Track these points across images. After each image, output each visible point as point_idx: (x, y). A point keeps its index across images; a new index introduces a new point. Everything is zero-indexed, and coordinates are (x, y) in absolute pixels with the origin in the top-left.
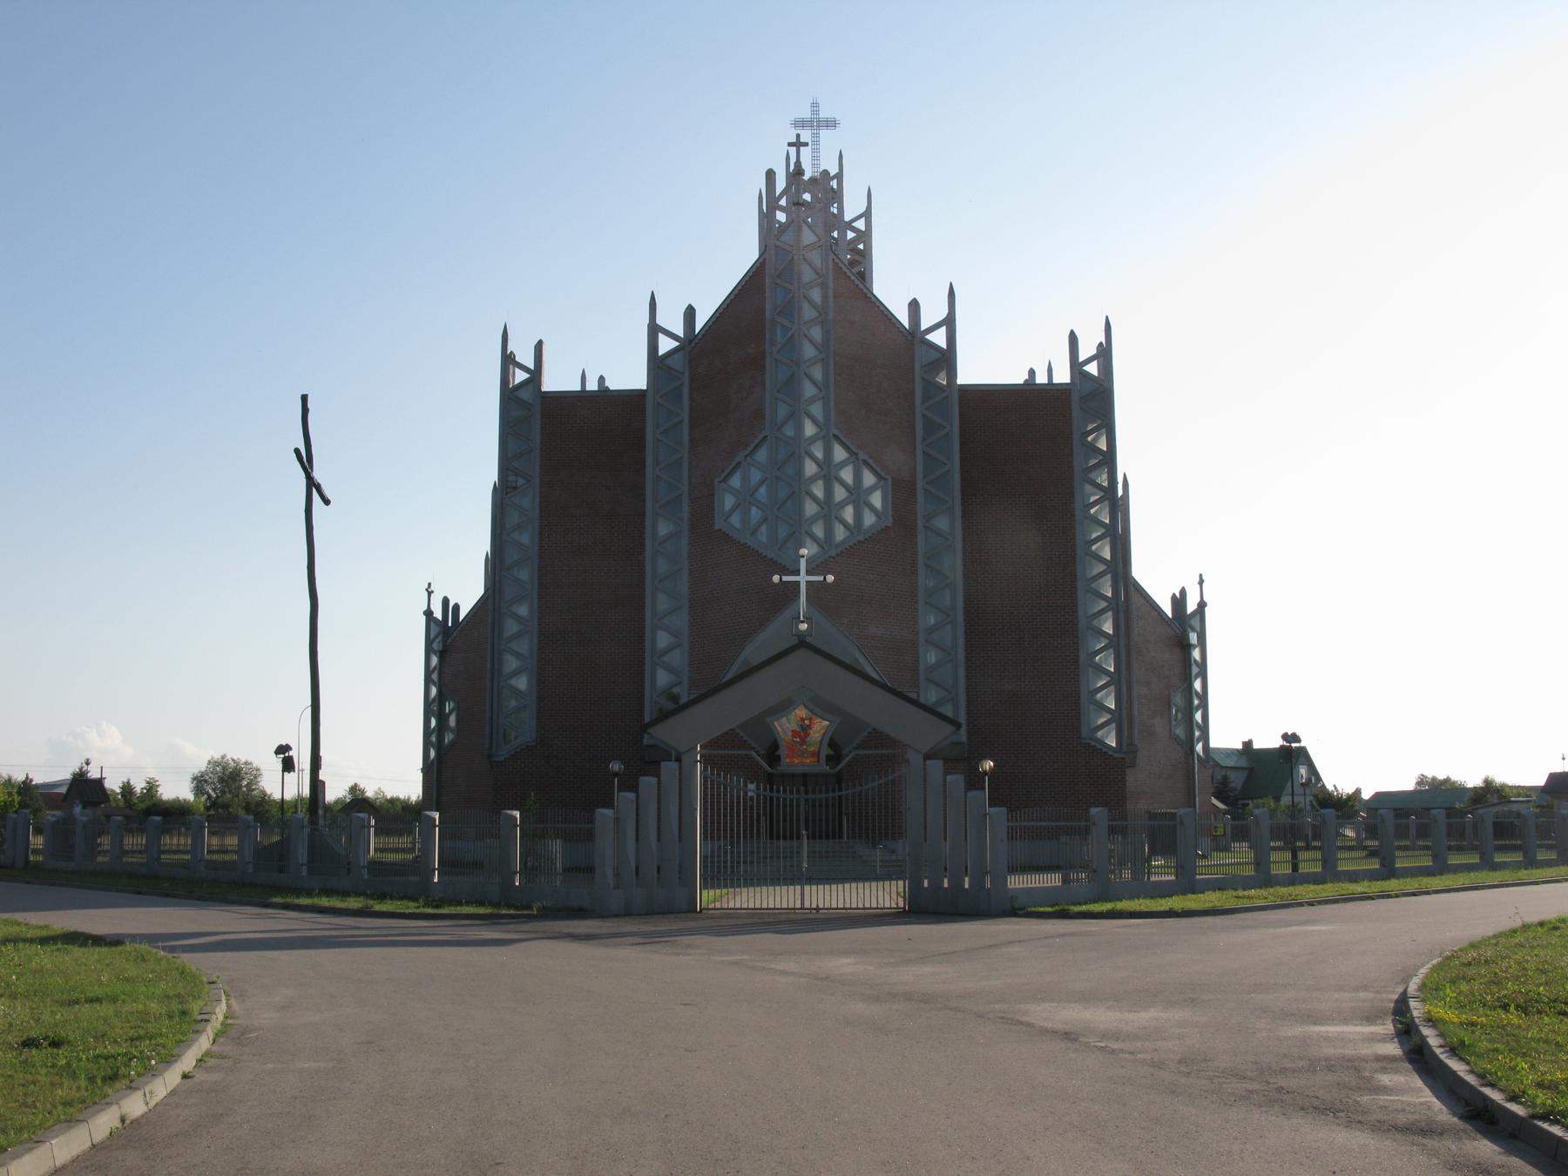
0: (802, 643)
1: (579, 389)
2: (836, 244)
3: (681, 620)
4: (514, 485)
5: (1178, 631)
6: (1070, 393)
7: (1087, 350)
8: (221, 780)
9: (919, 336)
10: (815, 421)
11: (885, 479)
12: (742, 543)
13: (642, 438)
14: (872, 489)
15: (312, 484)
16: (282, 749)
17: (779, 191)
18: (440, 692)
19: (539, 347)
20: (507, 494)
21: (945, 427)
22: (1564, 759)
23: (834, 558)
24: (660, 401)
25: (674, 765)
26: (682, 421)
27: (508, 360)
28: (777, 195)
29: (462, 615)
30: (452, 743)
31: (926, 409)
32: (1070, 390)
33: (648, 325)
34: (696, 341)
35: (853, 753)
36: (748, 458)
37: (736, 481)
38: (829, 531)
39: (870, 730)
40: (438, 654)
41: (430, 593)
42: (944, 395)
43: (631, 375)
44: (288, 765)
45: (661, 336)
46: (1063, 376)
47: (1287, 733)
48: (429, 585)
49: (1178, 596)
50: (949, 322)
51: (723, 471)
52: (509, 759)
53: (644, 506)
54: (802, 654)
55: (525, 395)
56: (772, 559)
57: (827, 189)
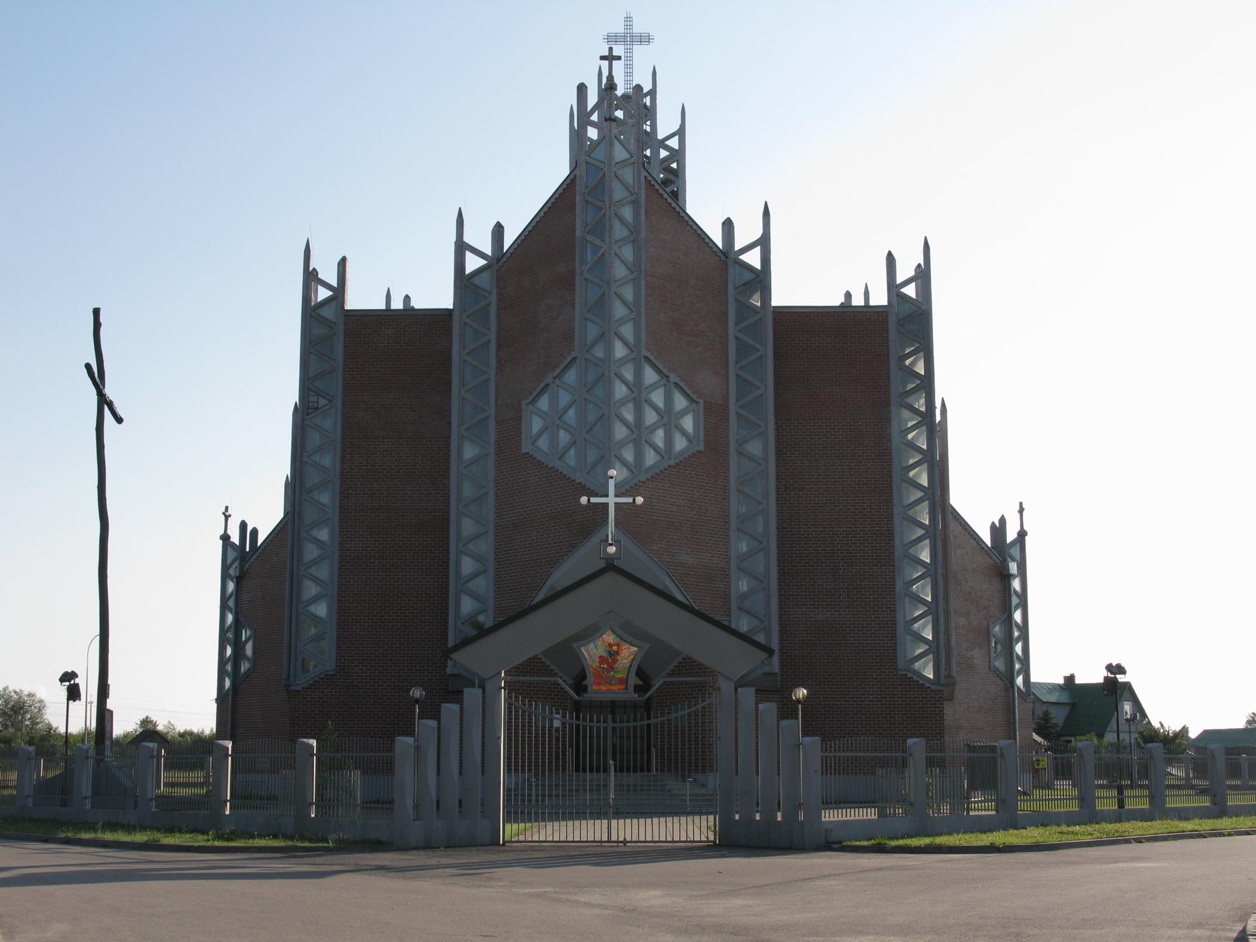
1: (383, 307)
2: (649, 163)
3: (485, 547)
4: (315, 405)
7: (905, 271)
9: (732, 256)
10: (625, 343)
12: (550, 466)
13: (448, 358)
14: (683, 413)
15: (104, 401)
16: (68, 677)
18: (236, 620)
19: (343, 263)
20: (308, 415)
24: (467, 321)
27: (311, 277)
28: (589, 109)
29: (261, 538)
32: (887, 312)
36: (556, 379)
37: (544, 403)
39: (683, 656)
40: (235, 580)
41: (227, 517)
45: (469, 255)
46: (880, 298)
49: (997, 524)
50: (764, 242)
52: (307, 688)
54: (610, 577)
55: (328, 313)
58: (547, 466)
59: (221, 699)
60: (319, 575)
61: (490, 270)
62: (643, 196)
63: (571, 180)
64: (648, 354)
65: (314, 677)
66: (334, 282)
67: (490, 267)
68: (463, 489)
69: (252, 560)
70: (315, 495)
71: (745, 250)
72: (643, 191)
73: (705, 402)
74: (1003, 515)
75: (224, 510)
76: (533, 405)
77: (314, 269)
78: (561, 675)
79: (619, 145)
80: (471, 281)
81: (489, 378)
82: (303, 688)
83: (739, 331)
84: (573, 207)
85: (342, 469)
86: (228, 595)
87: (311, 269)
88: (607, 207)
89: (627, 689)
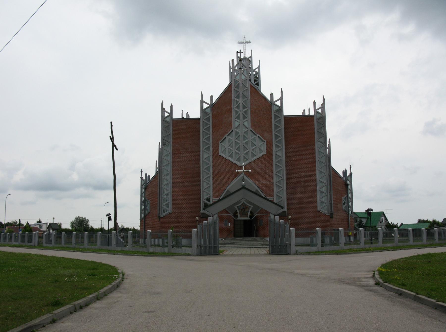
0: (244, 187)
1: (181, 118)
2: (251, 75)
4: (165, 144)
5: (344, 181)
6: (314, 117)
7: (318, 105)
8: (79, 223)
9: (273, 103)
11: (264, 141)
12: (226, 159)
13: (199, 131)
15: (114, 145)
16: (108, 215)
17: (235, 65)
18: (145, 199)
19: (171, 107)
21: (280, 127)
22: (54, 219)
23: (251, 163)
25: (211, 218)
26: (210, 126)
27: (163, 110)
28: (235, 66)
29: (151, 178)
30: (149, 213)
31: (275, 122)
32: (314, 117)
33: (201, 100)
34: (214, 105)
35: (256, 214)
39: (261, 208)
40: (144, 189)
41: (142, 172)
43: (196, 114)
44: (110, 219)
45: (204, 104)
46: (312, 113)
47: (372, 210)
48: (142, 170)
49: (344, 171)
50: (281, 99)
53: (200, 149)
54: (243, 190)
55: (168, 119)
56: (234, 163)
57: (249, 61)
58: (226, 159)
59: (141, 220)
61: (210, 108)
62: (249, 88)
63: (231, 84)
64: (251, 129)
66: (169, 111)
73: (266, 141)
74: (346, 169)
77: (164, 108)
78: (231, 213)
79: (243, 75)
83: (276, 142)
85: (173, 160)
86: (142, 193)
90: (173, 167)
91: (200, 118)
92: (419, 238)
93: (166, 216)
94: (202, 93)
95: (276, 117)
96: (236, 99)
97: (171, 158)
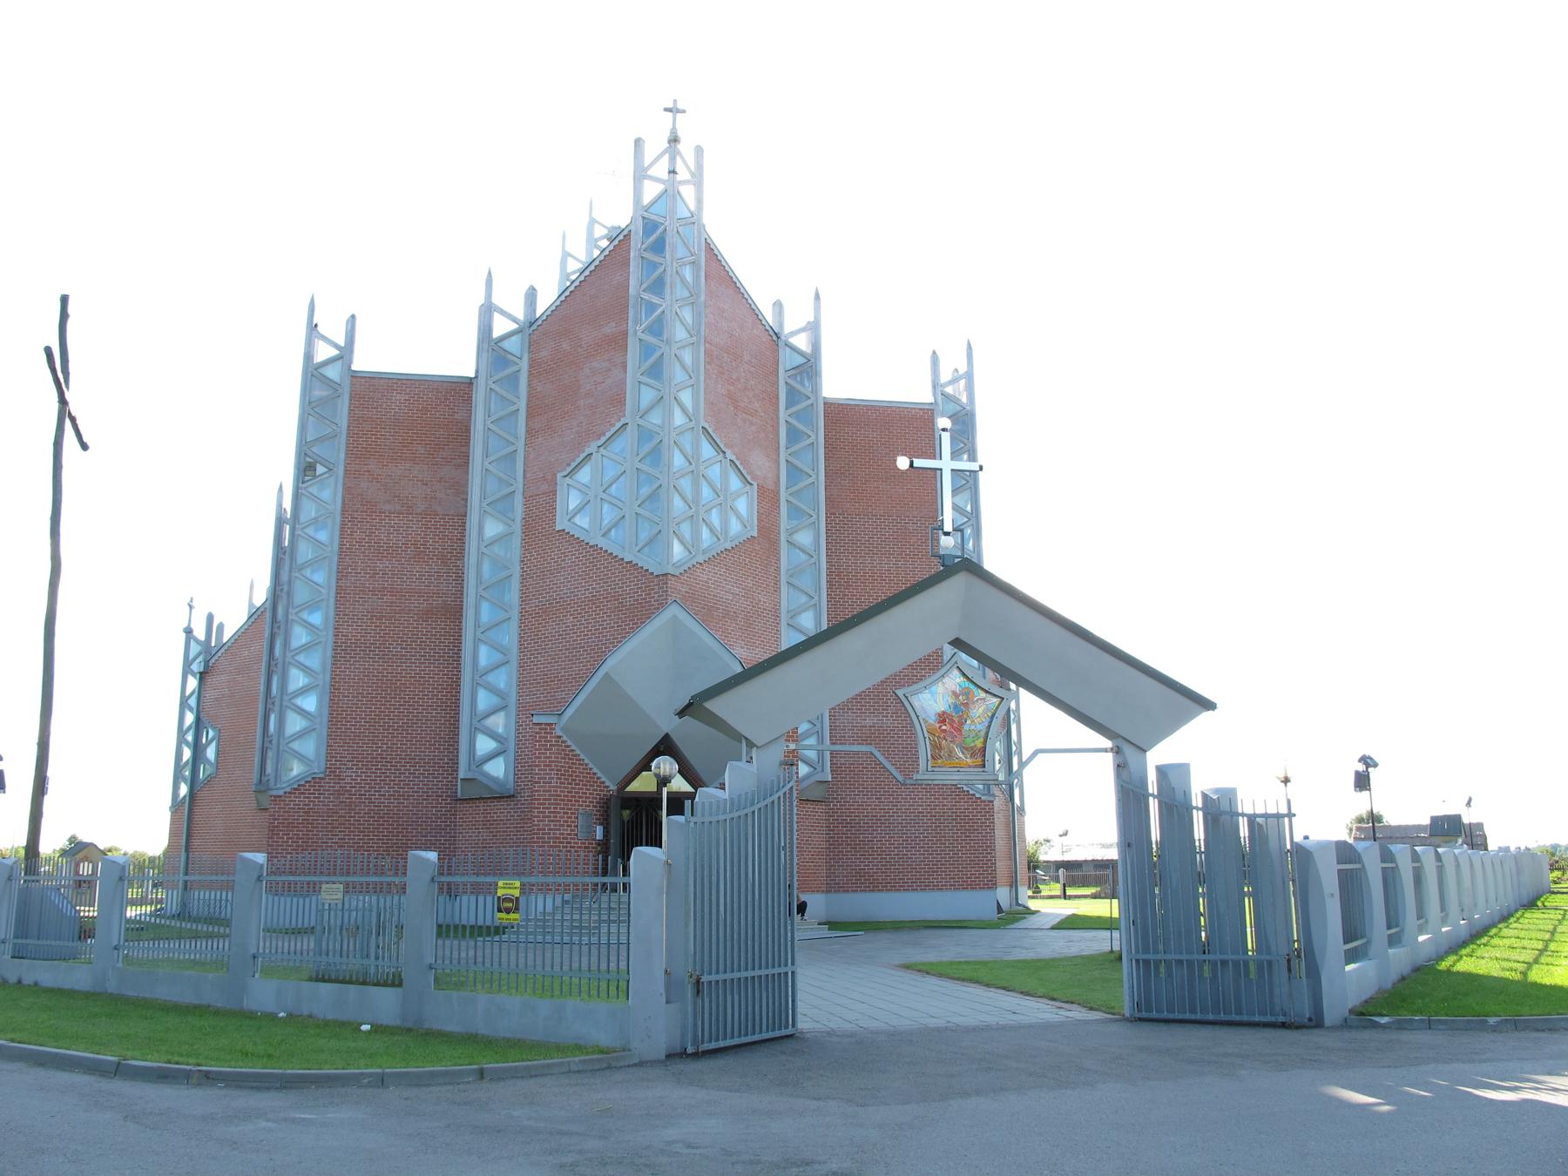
3: (509, 636)
9: (783, 338)
10: (684, 410)
12: (591, 544)
14: (738, 495)
18: (198, 720)
20: (303, 483)
24: (493, 386)
30: (209, 779)
36: (601, 449)
37: (584, 475)
38: (696, 534)
40: (198, 676)
42: (809, 402)
43: (459, 361)
50: (814, 328)
51: (569, 465)
52: (290, 793)
55: (333, 373)
60: (308, 663)
61: (520, 334)
64: (707, 426)
65: (299, 781)
67: (521, 331)
68: (479, 569)
69: (219, 654)
70: (308, 572)
71: (793, 333)
72: (703, 253)
75: (189, 601)
76: (571, 478)
80: (499, 344)
81: (516, 450)
82: (285, 793)
84: (626, 263)
85: (341, 545)
86: (188, 693)
87: (314, 323)
88: (669, 263)
89: (984, 766)
90: (341, 574)
91: (471, 379)
92: (1157, 892)
93: (295, 789)
94: (490, 273)
95: (793, 396)
96: (646, 296)
97: (337, 533)
